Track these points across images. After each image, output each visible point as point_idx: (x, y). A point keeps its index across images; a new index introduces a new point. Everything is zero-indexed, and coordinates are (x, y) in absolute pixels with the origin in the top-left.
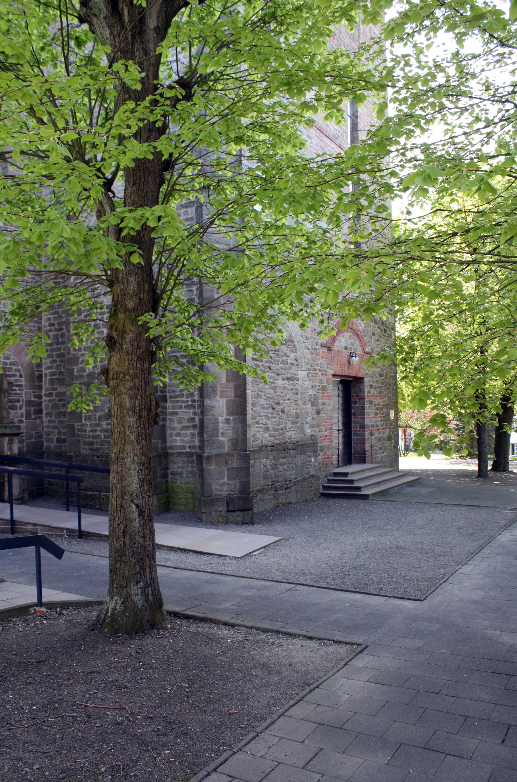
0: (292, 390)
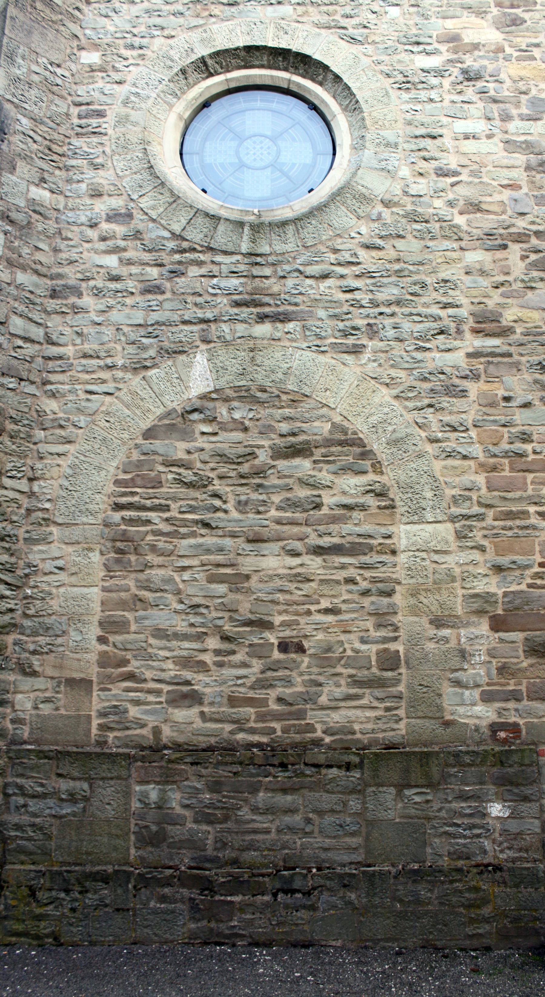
0: (350, 581)
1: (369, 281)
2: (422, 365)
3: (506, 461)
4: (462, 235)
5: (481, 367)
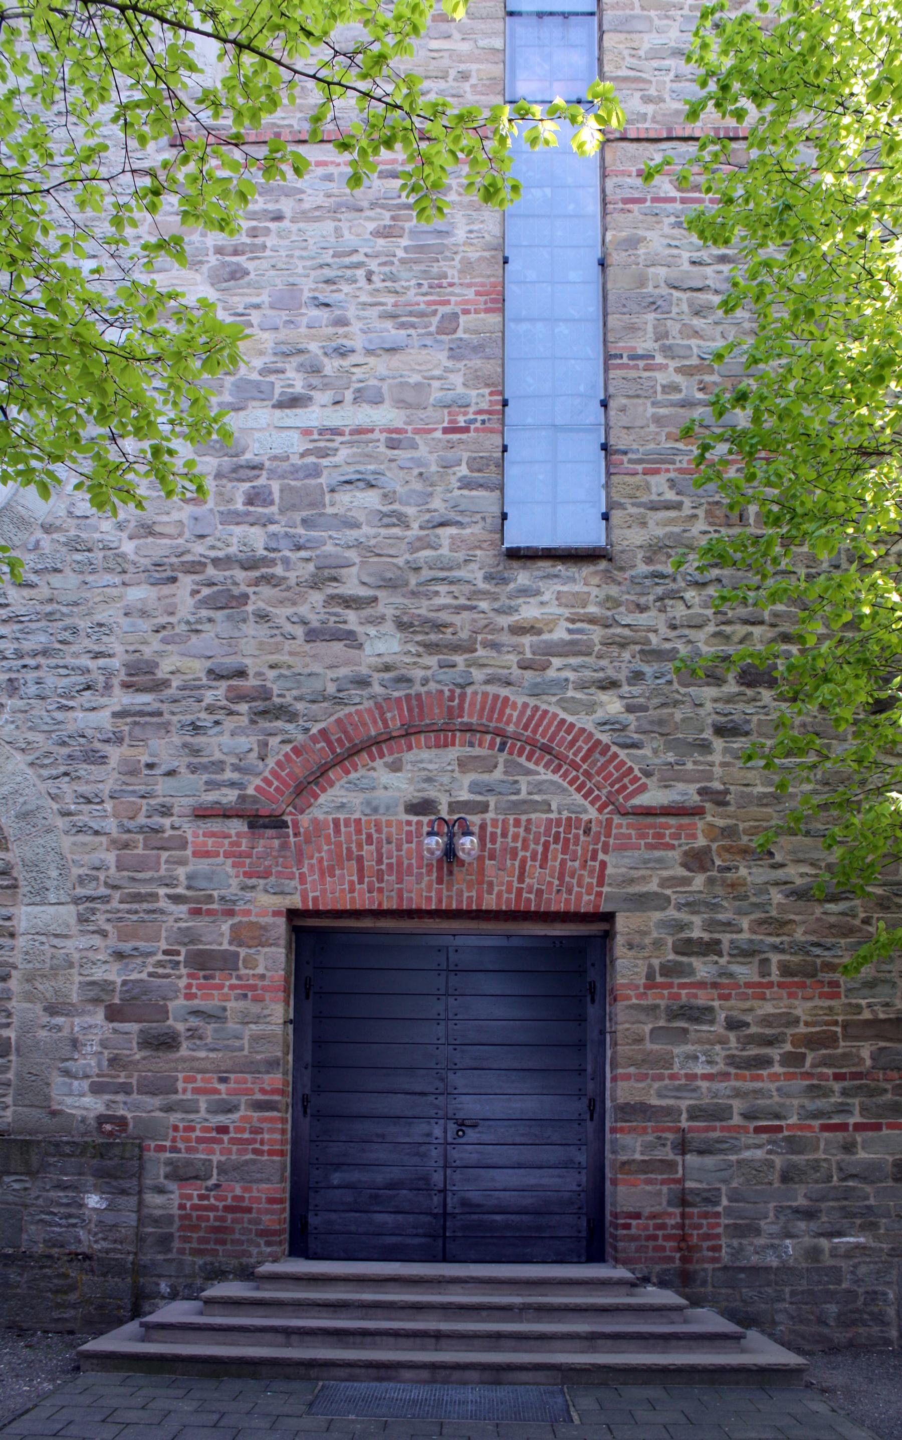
1: (17, 627)
2: (62, 727)
3: (141, 837)
4: (126, 566)
5: (126, 728)
